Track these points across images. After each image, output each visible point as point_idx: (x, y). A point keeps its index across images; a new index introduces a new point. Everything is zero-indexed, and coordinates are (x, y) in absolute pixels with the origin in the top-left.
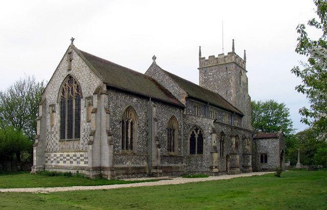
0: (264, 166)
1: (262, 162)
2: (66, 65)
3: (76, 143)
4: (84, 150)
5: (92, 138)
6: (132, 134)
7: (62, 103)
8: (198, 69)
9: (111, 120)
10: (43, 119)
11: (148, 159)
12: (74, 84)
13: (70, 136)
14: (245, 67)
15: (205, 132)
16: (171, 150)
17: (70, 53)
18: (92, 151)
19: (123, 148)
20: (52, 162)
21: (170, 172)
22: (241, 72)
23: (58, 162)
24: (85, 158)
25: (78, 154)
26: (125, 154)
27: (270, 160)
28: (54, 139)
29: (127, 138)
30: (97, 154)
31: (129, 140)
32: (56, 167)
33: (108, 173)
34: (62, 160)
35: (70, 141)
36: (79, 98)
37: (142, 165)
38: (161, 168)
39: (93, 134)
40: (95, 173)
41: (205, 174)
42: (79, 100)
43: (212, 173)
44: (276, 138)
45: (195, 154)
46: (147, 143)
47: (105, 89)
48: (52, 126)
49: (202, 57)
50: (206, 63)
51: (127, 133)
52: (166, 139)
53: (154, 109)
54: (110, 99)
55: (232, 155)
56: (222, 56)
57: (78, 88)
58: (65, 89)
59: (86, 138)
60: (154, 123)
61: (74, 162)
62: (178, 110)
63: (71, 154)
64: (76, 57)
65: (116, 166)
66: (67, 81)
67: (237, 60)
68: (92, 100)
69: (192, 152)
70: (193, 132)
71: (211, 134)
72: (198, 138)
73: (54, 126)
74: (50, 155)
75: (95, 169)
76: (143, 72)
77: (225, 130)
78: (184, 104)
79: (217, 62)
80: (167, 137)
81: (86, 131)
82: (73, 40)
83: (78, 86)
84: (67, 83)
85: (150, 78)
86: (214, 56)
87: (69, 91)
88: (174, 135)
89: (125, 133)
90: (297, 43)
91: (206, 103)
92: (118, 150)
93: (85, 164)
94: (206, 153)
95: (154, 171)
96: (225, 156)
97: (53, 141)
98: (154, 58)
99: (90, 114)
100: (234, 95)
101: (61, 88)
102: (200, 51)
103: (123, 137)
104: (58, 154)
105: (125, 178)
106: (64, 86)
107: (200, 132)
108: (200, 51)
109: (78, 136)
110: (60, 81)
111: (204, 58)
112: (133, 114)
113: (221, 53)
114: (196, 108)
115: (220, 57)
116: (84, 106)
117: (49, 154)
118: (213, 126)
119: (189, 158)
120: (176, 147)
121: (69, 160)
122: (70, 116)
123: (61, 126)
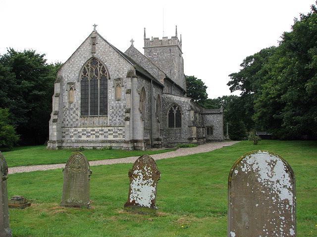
7: (84, 81)
13: (94, 113)
20: (71, 137)
23: (80, 137)
25: (106, 129)
27: (215, 133)
34: (85, 134)
36: (105, 79)
44: (220, 113)
48: (70, 103)
56: (166, 39)
58: (87, 70)
61: (100, 136)
76: (124, 52)
79: (162, 44)
81: (115, 108)
82: (95, 26)
84: (90, 65)
87: (92, 71)
94: (185, 127)
95: (156, 142)
97: (71, 117)
98: (132, 41)
101: (83, 68)
104: (80, 130)
107: (178, 108)
109: (104, 112)
110: (81, 62)
117: (67, 129)
121: (94, 134)
122: (94, 94)
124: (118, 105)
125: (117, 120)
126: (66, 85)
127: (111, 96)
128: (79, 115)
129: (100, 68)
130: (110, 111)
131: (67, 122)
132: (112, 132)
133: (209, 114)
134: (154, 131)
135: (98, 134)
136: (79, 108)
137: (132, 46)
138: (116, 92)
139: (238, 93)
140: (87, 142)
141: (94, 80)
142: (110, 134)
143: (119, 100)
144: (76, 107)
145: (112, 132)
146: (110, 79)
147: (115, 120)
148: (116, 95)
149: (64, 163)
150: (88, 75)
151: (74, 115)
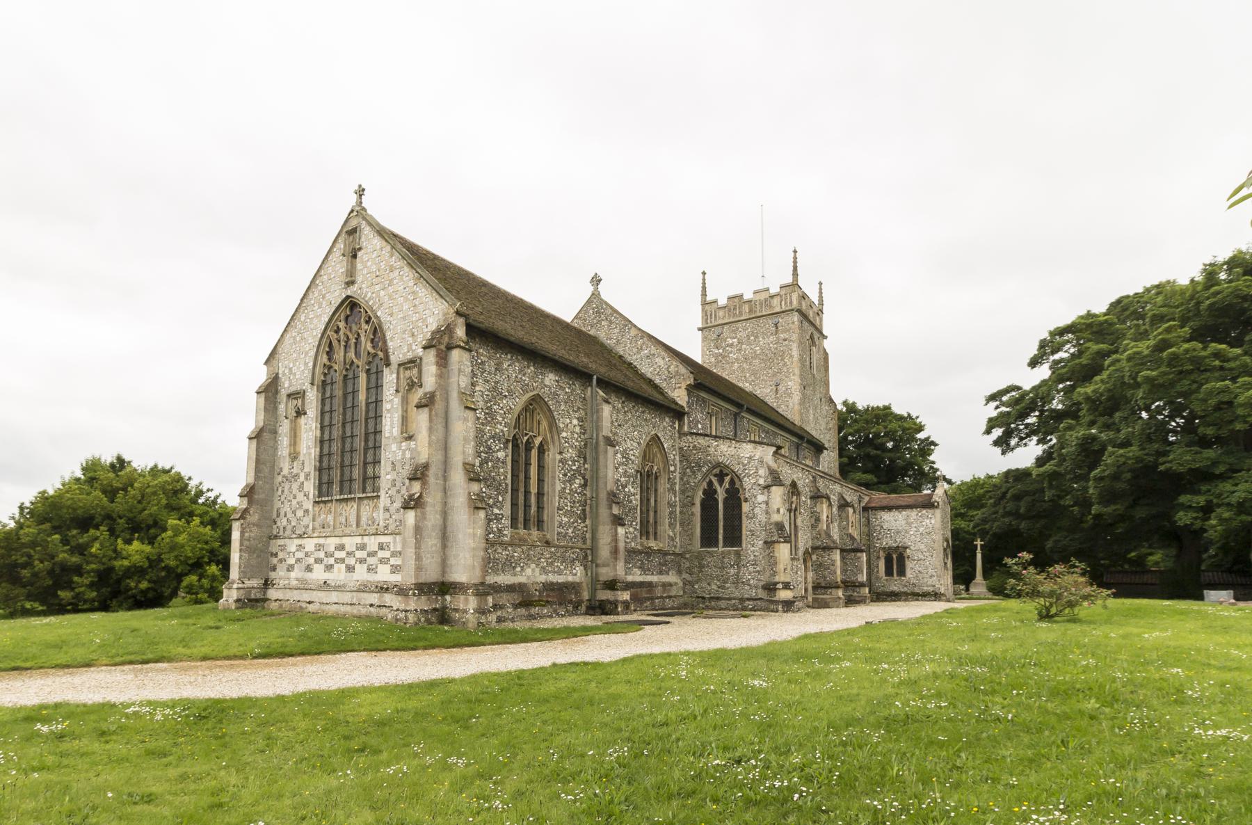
0: (895, 585)
1: (889, 572)
2: (339, 266)
3: (366, 510)
4: (392, 528)
5: (416, 487)
6: (541, 481)
8: (700, 329)
9: (479, 434)
11: (589, 557)
12: (364, 326)
13: (346, 484)
15: (748, 482)
16: (648, 533)
17: (352, 232)
18: (418, 530)
19: (514, 524)
20: (290, 568)
21: (648, 599)
23: (309, 569)
24: (394, 554)
25: (372, 543)
26: (522, 542)
28: (300, 497)
29: (527, 493)
30: (432, 542)
31: (533, 500)
32: (304, 586)
33: (468, 604)
36: (379, 358)
37: (570, 578)
38: (628, 586)
39: (419, 474)
40: (424, 604)
41: (750, 604)
42: (379, 373)
43: (777, 602)
44: (929, 504)
45: (716, 545)
46: (586, 511)
47: (460, 332)
49: (709, 299)
50: (721, 313)
51: (527, 478)
52: (636, 500)
53: (606, 410)
54: (478, 366)
55: (820, 552)
56: (763, 296)
57: (378, 334)
58: (335, 343)
59: (398, 492)
60: (606, 452)
61: (358, 566)
62: (667, 419)
63: (351, 543)
64: (371, 244)
65: (492, 579)
66: (342, 317)
67: (804, 304)
68: (420, 372)
69: (709, 538)
71: (767, 487)
72: (726, 500)
73: (301, 457)
74: (283, 548)
75: (423, 589)
76: (568, 317)
78: (685, 405)
79: (751, 311)
80: (638, 497)
84: (342, 325)
85: (579, 333)
86: (741, 296)
88: (656, 490)
89: (522, 476)
91: (739, 406)
92: (500, 531)
94: (752, 546)
96: (801, 553)
97: (294, 502)
99: (413, 411)
100: (797, 397)
103: (515, 491)
104: (310, 544)
105: (521, 617)
106: (333, 336)
107: (732, 482)
109: (369, 483)
111: (715, 302)
112: (544, 423)
113: (761, 287)
114: (714, 418)
118: (774, 465)
119: (700, 557)
121: (342, 561)
127: (392, 427)
128: (311, 496)
132: (386, 554)
133: (889, 508)
134: (604, 552)
136: (314, 475)
137: (595, 295)
139: (1027, 455)
142: (382, 561)
144: (306, 470)
146: (388, 364)
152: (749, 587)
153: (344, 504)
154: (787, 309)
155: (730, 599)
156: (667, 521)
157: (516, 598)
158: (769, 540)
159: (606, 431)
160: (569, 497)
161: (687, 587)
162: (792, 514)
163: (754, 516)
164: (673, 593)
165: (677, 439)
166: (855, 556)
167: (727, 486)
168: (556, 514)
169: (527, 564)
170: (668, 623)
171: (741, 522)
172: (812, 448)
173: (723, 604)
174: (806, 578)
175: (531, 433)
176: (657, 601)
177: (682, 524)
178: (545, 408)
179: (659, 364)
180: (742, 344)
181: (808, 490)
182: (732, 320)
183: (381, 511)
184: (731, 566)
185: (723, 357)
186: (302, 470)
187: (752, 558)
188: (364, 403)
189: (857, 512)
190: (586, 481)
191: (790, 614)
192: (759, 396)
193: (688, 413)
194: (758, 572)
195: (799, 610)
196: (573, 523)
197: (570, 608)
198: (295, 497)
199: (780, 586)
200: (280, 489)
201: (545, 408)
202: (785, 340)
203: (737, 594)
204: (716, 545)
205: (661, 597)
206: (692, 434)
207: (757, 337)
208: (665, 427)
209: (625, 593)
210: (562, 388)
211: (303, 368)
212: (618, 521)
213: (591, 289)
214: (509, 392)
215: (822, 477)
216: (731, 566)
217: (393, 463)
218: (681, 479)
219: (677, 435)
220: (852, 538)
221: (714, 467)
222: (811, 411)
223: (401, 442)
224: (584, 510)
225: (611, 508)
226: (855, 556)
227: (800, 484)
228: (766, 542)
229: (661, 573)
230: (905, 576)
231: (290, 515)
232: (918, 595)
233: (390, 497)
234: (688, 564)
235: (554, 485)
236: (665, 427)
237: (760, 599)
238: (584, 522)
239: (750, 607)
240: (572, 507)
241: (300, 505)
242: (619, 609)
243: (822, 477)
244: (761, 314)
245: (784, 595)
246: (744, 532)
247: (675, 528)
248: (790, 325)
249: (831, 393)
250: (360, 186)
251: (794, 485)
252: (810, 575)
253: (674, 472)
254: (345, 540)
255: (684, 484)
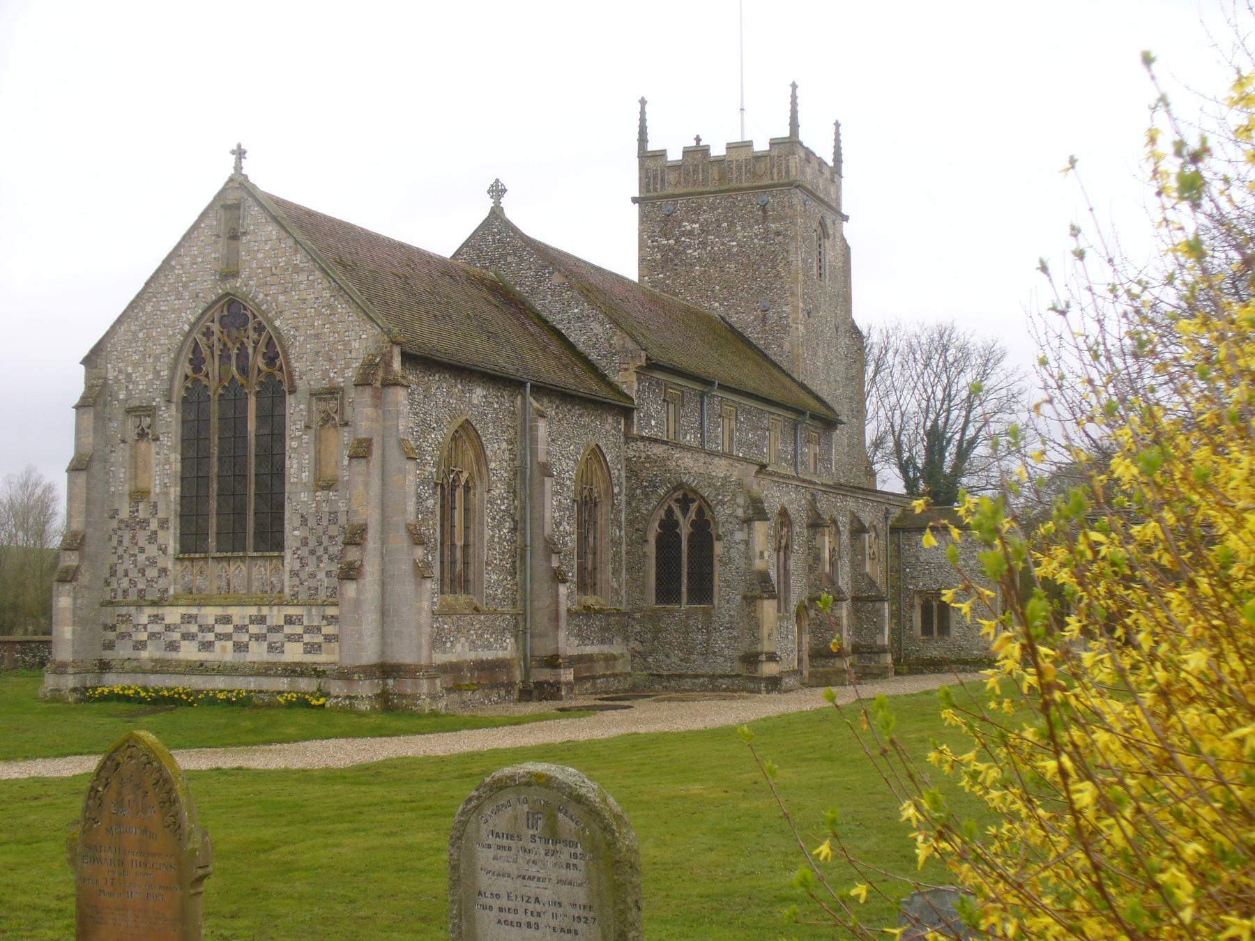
3: (262, 571)
4: (303, 597)
8: (634, 200)
10: (96, 465)
13: (233, 543)
14: (838, 199)
15: (722, 513)
20: (141, 645)
22: (822, 224)
23: (173, 646)
24: (308, 630)
25: (276, 616)
31: (459, 554)
35: (229, 559)
37: (501, 654)
41: (724, 683)
43: (759, 679)
45: (679, 601)
49: (652, 146)
56: (742, 155)
58: (205, 352)
61: (253, 644)
62: (610, 420)
66: (217, 318)
69: (667, 591)
70: (670, 512)
77: (791, 502)
79: (722, 178)
80: (575, 537)
81: (312, 522)
83: (270, 341)
84: (216, 327)
85: (481, 282)
87: (225, 358)
90: (1077, 164)
91: (707, 382)
93: (307, 652)
94: (727, 599)
96: (793, 609)
97: (141, 558)
98: (497, 191)
101: (189, 345)
102: (643, 120)
104: (173, 615)
106: (199, 337)
107: (700, 511)
108: (643, 120)
115: (734, 157)
116: (301, 425)
117: (124, 611)
119: (654, 617)
120: (606, 576)
121: (228, 637)
123: (182, 497)
124: (325, 508)
125: (321, 575)
126: (120, 417)
127: (301, 468)
128: (171, 551)
129: (256, 343)
130: (293, 533)
131: (125, 583)
132: (299, 630)
134: (541, 621)
135: (245, 638)
136: (174, 524)
137: (496, 214)
138: (318, 452)
140: (201, 668)
141: (233, 398)
142: (290, 638)
143: (328, 488)
144: (161, 515)
145: (299, 630)
146: (293, 391)
147: (313, 575)
148: (318, 462)
149: (96, 753)
150: (207, 376)
151: (152, 550)
152: (722, 659)
153: (225, 564)
154: (781, 181)
155: (696, 676)
156: (610, 567)
157: (449, 680)
158: (749, 594)
159: (542, 457)
160: (497, 547)
161: (637, 660)
162: (782, 554)
163: (730, 560)
164: (618, 669)
165: (622, 445)
166: (874, 607)
167: (694, 517)
168: (485, 572)
169: (457, 638)
170: (629, 707)
171: (712, 568)
172: (820, 425)
173: (687, 683)
174: (800, 644)
175: (458, 469)
176: (599, 681)
177: (630, 569)
178: (473, 434)
179: (595, 331)
180: (708, 233)
181: (804, 515)
182: (690, 189)
183: (287, 576)
184: (699, 629)
185: (676, 254)
186: (154, 514)
187: (727, 618)
188: (253, 435)
189: (882, 536)
190: (516, 522)
191: (775, 695)
192: (736, 326)
193: (637, 409)
194: (735, 638)
195: (788, 691)
196: (502, 581)
197: (503, 693)
198: (142, 550)
199: (763, 658)
200: (115, 538)
201: (473, 434)
202: (778, 234)
203: (706, 669)
204: (679, 601)
205: (604, 676)
206: (642, 438)
207: (732, 224)
208: (607, 432)
209: (568, 671)
210: (490, 404)
211: (150, 377)
212: (558, 577)
213: (489, 203)
214: (437, 423)
215: (825, 492)
216: (699, 629)
217: (302, 517)
218: (629, 504)
219: (622, 440)
220: (872, 583)
221: (675, 489)
222: (820, 353)
223: (316, 491)
224: (514, 562)
225: (550, 561)
226: (874, 607)
227: (792, 510)
228: (745, 597)
229: (602, 642)
230: (949, 635)
231: (133, 574)
232: (966, 663)
233: (301, 559)
234: (637, 628)
235: (482, 533)
236: (607, 432)
237: (737, 676)
238: (513, 579)
239: (724, 686)
240: (501, 560)
241: (152, 562)
242: (563, 693)
243: (825, 492)
244: (738, 185)
245: (769, 669)
246: (716, 582)
247: (620, 575)
248: (787, 210)
249: (854, 316)
250: (239, 146)
251: (784, 513)
252: (806, 638)
253: (619, 493)
254: (232, 611)
255: (633, 512)
